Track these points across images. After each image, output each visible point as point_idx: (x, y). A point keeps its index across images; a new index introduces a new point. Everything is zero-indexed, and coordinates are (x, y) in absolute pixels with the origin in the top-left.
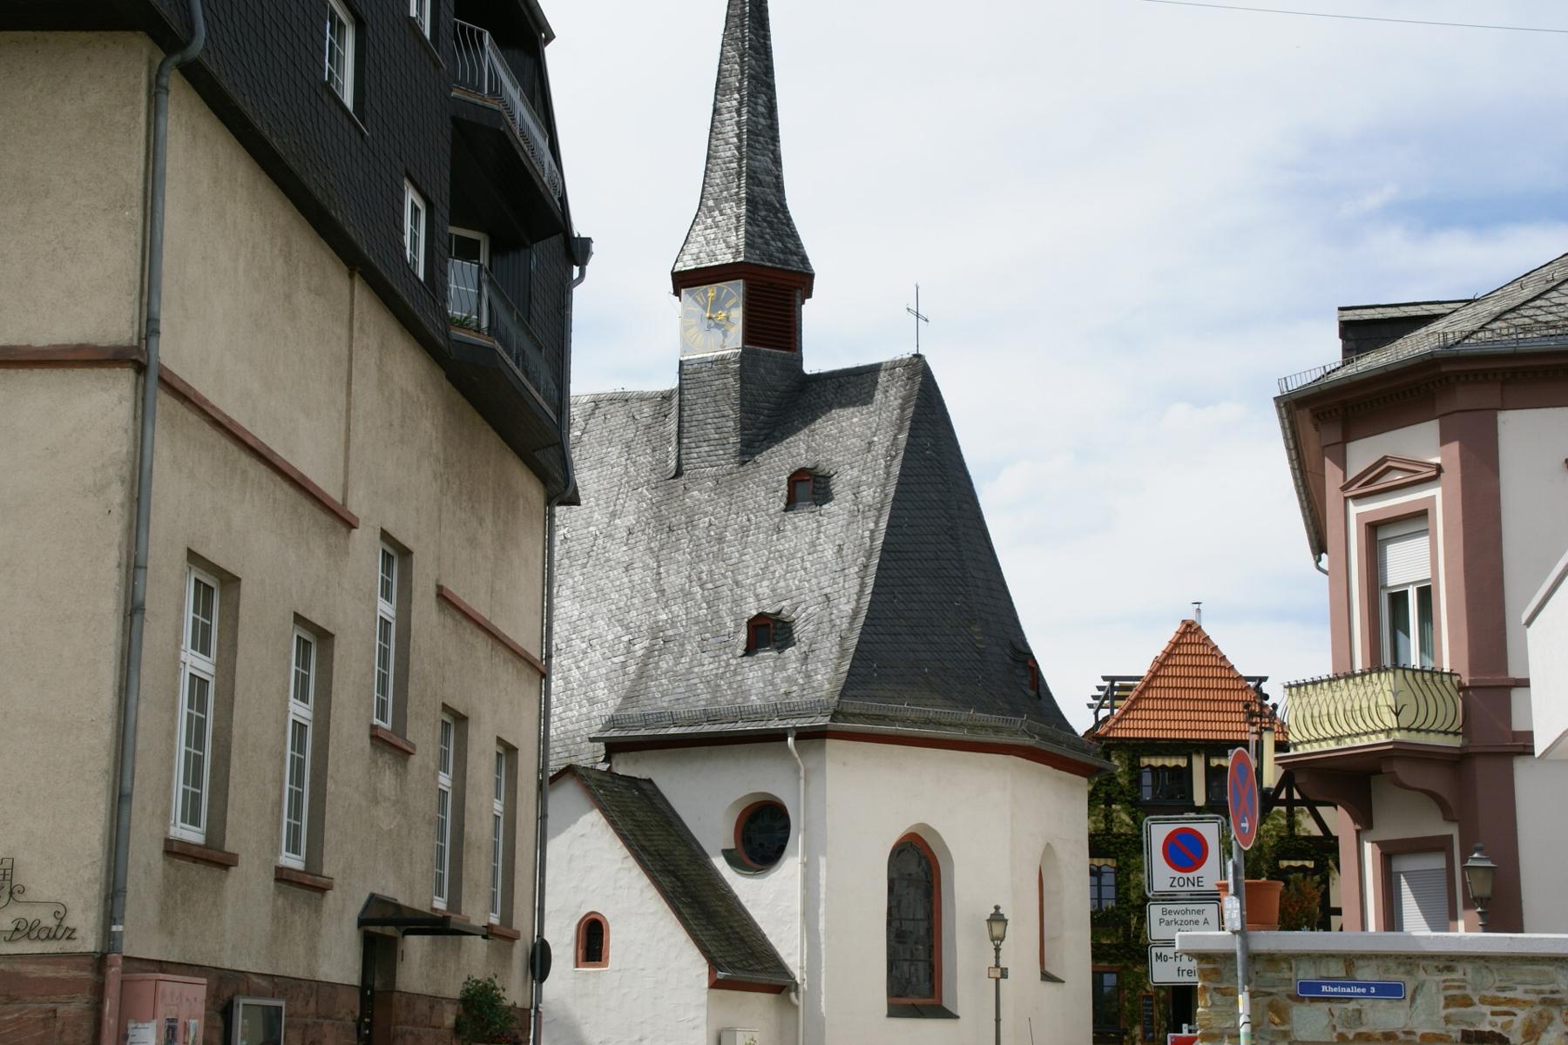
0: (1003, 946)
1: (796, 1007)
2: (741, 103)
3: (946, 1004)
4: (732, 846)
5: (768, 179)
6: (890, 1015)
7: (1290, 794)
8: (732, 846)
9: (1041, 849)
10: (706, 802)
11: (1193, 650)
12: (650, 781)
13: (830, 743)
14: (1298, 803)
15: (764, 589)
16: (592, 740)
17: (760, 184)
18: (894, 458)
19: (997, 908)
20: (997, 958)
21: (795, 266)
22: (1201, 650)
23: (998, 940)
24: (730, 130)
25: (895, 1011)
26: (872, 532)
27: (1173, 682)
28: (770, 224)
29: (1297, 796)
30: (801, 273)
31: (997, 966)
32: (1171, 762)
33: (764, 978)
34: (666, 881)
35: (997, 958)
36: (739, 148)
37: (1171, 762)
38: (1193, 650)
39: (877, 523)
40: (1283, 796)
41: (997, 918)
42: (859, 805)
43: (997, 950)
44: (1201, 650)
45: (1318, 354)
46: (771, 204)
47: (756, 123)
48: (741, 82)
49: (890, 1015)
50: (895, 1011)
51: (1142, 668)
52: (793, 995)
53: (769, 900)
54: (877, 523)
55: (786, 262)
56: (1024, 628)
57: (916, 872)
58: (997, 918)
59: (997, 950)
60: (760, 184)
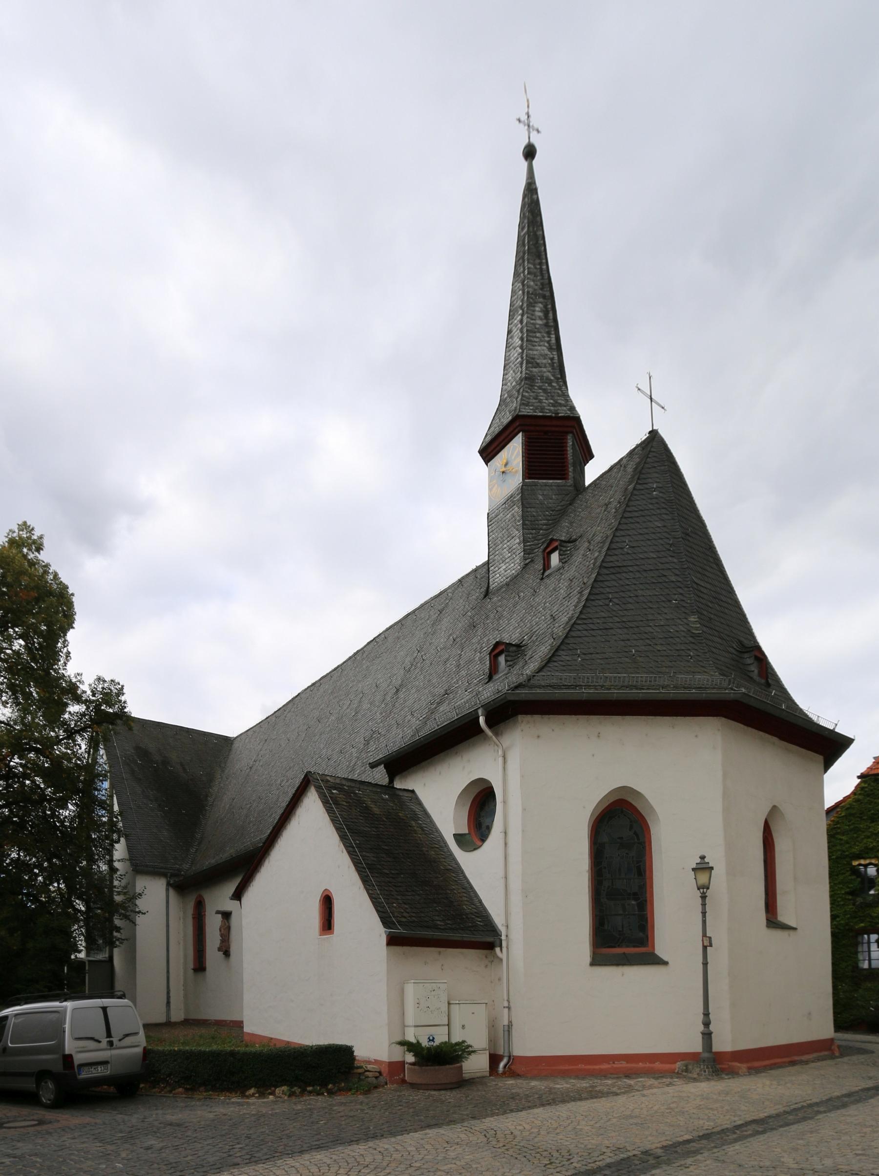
1: (501, 960)
2: (522, 315)
4: (465, 830)
5: (544, 361)
6: (593, 963)
8: (465, 830)
10: (439, 794)
12: (413, 791)
17: (538, 365)
18: (247, 1103)
19: (703, 858)
21: (563, 412)
24: (517, 334)
28: (545, 391)
34: (486, 822)
36: (521, 347)
41: (703, 867)
42: (542, 789)
43: (704, 897)
45: (694, 866)
46: (548, 378)
47: (534, 324)
49: (593, 963)
52: (498, 950)
53: (480, 869)
57: (620, 837)
58: (703, 867)
59: (704, 897)
60: (538, 365)
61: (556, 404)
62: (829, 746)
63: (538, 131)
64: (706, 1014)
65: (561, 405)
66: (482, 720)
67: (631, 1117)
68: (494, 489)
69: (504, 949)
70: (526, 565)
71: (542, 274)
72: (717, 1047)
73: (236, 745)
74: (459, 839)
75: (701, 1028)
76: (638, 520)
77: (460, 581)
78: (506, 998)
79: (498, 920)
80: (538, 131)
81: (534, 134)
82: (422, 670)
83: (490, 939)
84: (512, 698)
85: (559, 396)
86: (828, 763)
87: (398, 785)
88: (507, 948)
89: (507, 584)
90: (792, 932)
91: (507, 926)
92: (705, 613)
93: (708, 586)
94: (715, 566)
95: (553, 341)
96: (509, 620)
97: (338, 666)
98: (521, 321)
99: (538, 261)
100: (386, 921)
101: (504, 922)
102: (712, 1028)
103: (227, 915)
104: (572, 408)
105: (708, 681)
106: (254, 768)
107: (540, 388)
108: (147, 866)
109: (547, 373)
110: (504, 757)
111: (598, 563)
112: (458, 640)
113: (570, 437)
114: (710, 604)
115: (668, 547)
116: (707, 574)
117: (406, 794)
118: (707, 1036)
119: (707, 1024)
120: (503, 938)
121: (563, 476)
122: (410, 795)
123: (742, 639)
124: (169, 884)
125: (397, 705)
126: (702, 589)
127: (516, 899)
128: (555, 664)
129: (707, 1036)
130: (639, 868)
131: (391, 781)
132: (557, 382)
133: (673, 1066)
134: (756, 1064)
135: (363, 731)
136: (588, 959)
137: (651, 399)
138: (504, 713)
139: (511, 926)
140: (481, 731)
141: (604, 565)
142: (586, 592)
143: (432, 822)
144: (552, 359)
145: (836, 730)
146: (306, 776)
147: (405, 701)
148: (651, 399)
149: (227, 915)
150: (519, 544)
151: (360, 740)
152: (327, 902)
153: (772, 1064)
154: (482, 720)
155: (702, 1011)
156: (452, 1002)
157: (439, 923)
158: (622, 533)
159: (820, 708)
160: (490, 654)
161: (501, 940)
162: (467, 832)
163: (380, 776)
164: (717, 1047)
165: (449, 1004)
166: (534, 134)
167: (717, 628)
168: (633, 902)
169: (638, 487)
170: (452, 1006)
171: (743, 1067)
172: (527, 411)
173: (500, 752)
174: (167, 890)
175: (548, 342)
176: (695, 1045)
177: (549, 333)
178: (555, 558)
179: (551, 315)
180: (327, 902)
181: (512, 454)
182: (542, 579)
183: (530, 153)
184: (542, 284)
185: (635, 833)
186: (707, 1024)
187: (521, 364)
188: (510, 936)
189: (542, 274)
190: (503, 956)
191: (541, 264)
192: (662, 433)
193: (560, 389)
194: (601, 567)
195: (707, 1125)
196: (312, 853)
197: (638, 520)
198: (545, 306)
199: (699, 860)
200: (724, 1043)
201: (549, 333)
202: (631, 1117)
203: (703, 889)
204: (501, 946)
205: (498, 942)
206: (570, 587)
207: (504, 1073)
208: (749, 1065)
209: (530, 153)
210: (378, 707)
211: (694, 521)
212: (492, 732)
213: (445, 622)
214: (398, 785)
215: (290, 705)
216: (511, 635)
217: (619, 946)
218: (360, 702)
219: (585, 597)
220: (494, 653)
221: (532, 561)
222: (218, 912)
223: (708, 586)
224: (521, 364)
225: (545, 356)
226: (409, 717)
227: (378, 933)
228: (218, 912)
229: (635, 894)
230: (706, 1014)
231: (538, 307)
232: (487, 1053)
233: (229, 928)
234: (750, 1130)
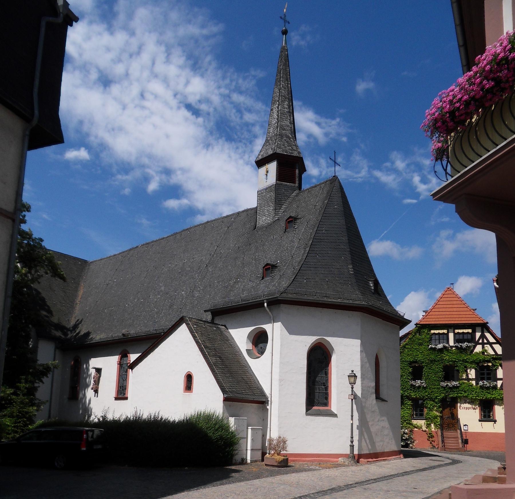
0: (355, 386)
2: (279, 105)
7: (483, 341)
9: (185, 113)
11: (449, 296)
13: (282, 305)
14: (486, 344)
16: (205, 311)
19: (353, 371)
21: (295, 154)
22: (452, 296)
26: (311, 233)
27: (442, 306)
28: (287, 142)
29: (485, 341)
32: (441, 331)
33: (257, 399)
34: (213, 360)
36: (278, 119)
37: (441, 331)
38: (449, 296)
40: (481, 341)
44: (452, 296)
48: (279, 98)
50: (101, 369)
60: (284, 130)
61: (292, 149)
63: (281, 18)
66: (265, 304)
67: (328, 477)
69: (269, 405)
73: (92, 267)
79: (267, 392)
80: (289, 23)
81: (287, 24)
83: (264, 400)
99: (286, 82)
101: (270, 393)
105: (356, 297)
111: (312, 236)
120: (269, 399)
127: (276, 383)
130: (326, 372)
131: (213, 319)
134: (370, 460)
138: (275, 303)
142: (308, 249)
144: (291, 128)
145: (405, 317)
149: (99, 371)
152: (189, 378)
154: (265, 304)
155: (350, 436)
158: (322, 223)
169: (329, 202)
172: (279, 151)
174: (55, 351)
175: (290, 120)
176: (348, 452)
180: (189, 378)
187: (277, 127)
195: (357, 480)
198: (289, 103)
201: (290, 116)
202: (328, 477)
207: (252, 461)
216: (270, 258)
224: (277, 127)
225: (288, 126)
229: (324, 383)
234: (371, 481)
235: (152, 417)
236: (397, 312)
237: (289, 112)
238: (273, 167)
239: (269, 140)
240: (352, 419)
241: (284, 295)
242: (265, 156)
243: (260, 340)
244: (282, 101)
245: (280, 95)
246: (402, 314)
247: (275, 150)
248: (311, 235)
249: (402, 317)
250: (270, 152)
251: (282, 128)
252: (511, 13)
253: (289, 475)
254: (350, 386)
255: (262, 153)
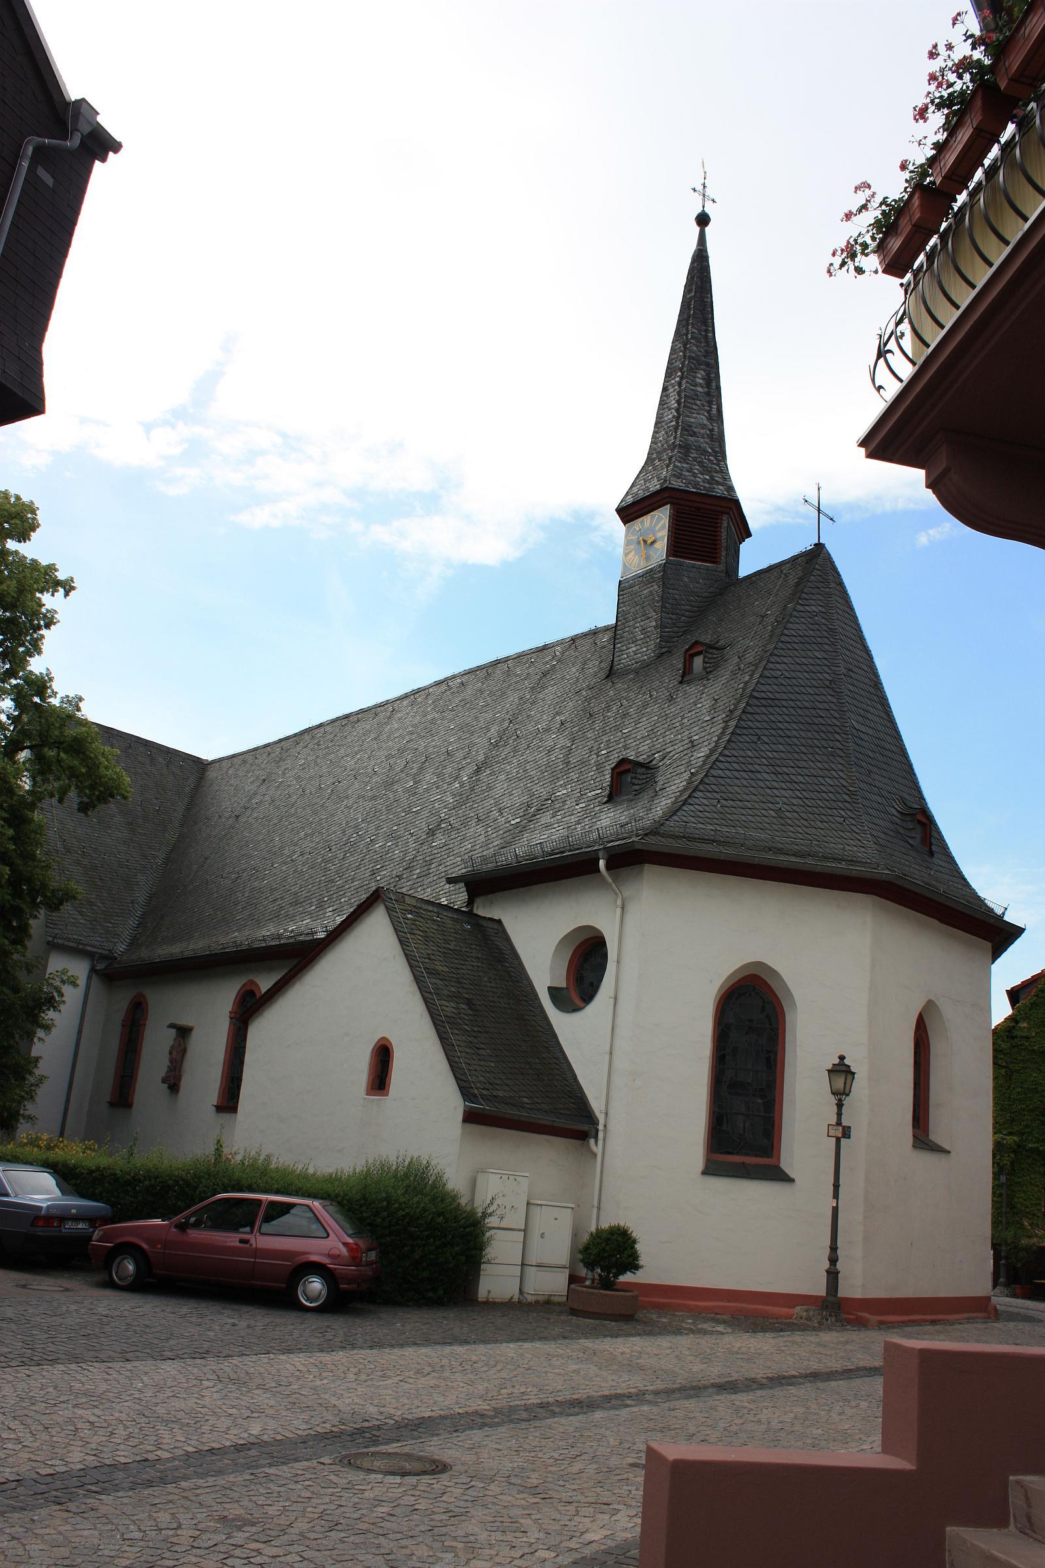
0: (847, 1101)
1: (595, 1155)
2: (682, 378)
3: (784, 1165)
4: (562, 983)
6: (706, 1172)
8: (562, 983)
10: (538, 935)
12: (499, 922)
15: (644, 748)
17: (694, 434)
19: (842, 1058)
20: (839, 1114)
21: (720, 490)
23: (841, 1096)
25: (712, 1169)
28: (701, 463)
30: (725, 498)
31: (839, 1123)
35: (839, 1114)
36: (677, 410)
39: (751, 676)
41: (841, 1070)
43: (840, 1105)
45: (830, 1067)
48: (683, 364)
49: (706, 1172)
50: (712, 1169)
51: (608, 617)
52: (592, 1141)
53: (578, 1034)
54: (751, 676)
55: (712, 490)
56: (916, 771)
57: (750, 1019)
58: (841, 1070)
59: (840, 1105)
60: (694, 434)
61: (712, 481)
62: (998, 934)
63: (714, 201)
64: (834, 1248)
65: (718, 483)
66: (602, 863)
67: (737, 1353)
68: (630, 555)
69: (600, 1143)
70: (663, 654)
71: (707, 342)
72: (843, 1292)
73: (211, 774)
74: (554, 992)
75: (827, 1265)
76: (796, 646)
77: (573, 639)
78: (596, 1204)
79: (596, 1104)
80: (714, 201)
82: (515, 751)
83: (585, 1128)
84: (640, 847)
85: (717, 472)
86: (996, 953)
87: (483, 910)
88: (604, 1140)
89: (636, 671)
90: (943, 1156)
91: (606, 1114)
92: (864, 764)
93: (870, 732)
94: (879, 706)
95: (714, 411)
96: (637, 722)
97: (387, 702)
98: (680, 384)
100: (466, 1091)
101: (603, 1108)
102: (839, 1265)
103: (183, 1032)
104: (731, 489)
105: (862, 849)
106: (243, 819)
107: (695, 459)
108: (69, 940)
109: (704, 444)
110: (623, 908)
112: (568, 725)
113: (725, 517)
114: (870, 754)
115: (827, 683)
116: (869, 716)
117: (490, 925)
118: (833, 1275)
119: (833, 1260)
120: (601, 1127)
121: (713, 558)
122: (496, 926)
123: (907, 797)
124: (93, 970)
125: (478, 790)
126: (862, 735)
128: (691, 808)
129: (833, 1275)
130: (768, 1059)
131: (470, 902)
132: (715, 457)
133: (790, 1311)
135: (425, 813)
136: (699, 1163)
137: (819, 510)
138: (628, 858)
139: (611, 1112)
140: (598, 871)
141: (755, 694)
142: (733, 723)
143: (521, 964)
144: (711, 430)
145: (1006, 918)
146: (377, 890)
147: (490, 788)
148: (819, 510)
150: (655, 627)
151: (422, 825)
152: (383, 1055)
153: (909, 1321)
154: (602, 863)
156: (532, 1201)
157: (525, 1100)
159: (992, 883)
160: (613, 769)
161: (597, 1131)
162: (564, 986)
163: (458, 897)
164: (843, 1292)
165: (528, 1204)
166: (708, 204)
167: (877, 784)
168: (760, 1101)
170: (532, 1207)
171: (874, 1318)
172: (677, 484)
173: (619, 902)
174: (89, 978)
175: (708, 412)
176: (821, 1291)
177: (710, 403)
178: (698, 662)
179: (714, 384)
180: (383, 1055)
181: (656, 525)
182: (681, 682)
183: (703, 220)
184: (706, 351)
185: (767, 1016)
186: (833, 1260)
187: (676, 428)
188: (609, 1127)
189: (707, 342)
190: (598, 1150)
191: (706, 331)
192: (830, 548)
193: (718, 465)
194: (751, 696)
196: (368, 988)
197: (796, 646)
198: (708, 375)
199: (837, 1061)
200: (853, 1286)
203: (841, 1096)
204: (596, 1137)
205: (593, 1132)
206: (713, 708)
208: (881, 1318)
209: (703, 220)
210: (449, 784)
211: (858, 652)
212: (610, 875)
213: (551, 693)
214: (481, 911)
215: (306, 737)
217: (738, 1154)
218: (421, 768)
219: (730, 730)
220: (618, 770)
221: (669, 652)
222: (172, 1026)
223: (870, 732)
224: (676, 428)
225: (703, 426)
226: (495, 814)
227: (452, 1103)
228: (172, 1026)
230: (834, 1248)
231: (701, 374)
232: (567, 1271)
233: (185, 1050)
235: (262, 1157)
236: (981, 901)
237: (708, 394)
238: (659, 523)
239: (654, 460)
240: (836, 1195)
241: (651, 840)
242: (641, 495)
243: (588, 958)
244: (691, 370)
245: (685, 356)
246: (999, 911)
247: (665, 481)
248: (744, 689)
249: (1000, 918)
250: (655, 486)
251: (688, 429)
252: (48, 335)
253: (620, 1340)
254: (833, 1100)
255: (635, 490)
